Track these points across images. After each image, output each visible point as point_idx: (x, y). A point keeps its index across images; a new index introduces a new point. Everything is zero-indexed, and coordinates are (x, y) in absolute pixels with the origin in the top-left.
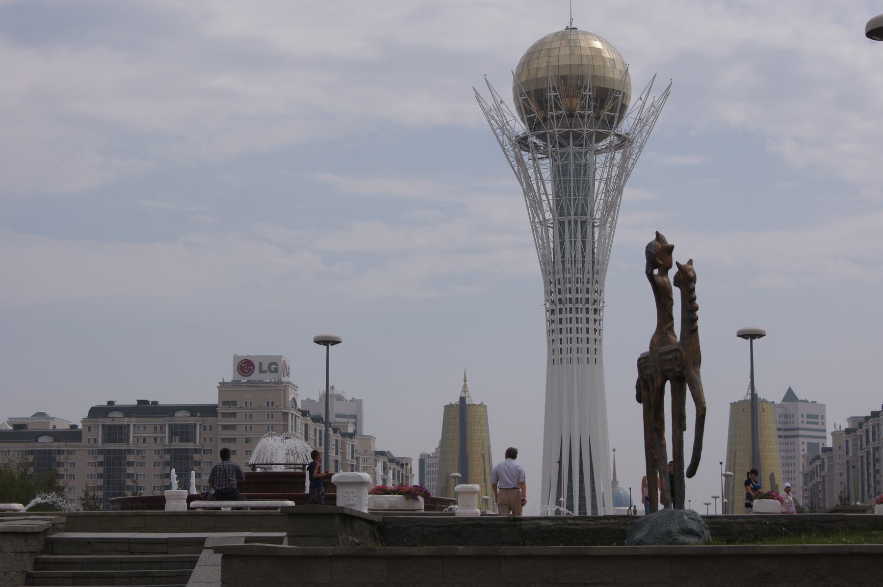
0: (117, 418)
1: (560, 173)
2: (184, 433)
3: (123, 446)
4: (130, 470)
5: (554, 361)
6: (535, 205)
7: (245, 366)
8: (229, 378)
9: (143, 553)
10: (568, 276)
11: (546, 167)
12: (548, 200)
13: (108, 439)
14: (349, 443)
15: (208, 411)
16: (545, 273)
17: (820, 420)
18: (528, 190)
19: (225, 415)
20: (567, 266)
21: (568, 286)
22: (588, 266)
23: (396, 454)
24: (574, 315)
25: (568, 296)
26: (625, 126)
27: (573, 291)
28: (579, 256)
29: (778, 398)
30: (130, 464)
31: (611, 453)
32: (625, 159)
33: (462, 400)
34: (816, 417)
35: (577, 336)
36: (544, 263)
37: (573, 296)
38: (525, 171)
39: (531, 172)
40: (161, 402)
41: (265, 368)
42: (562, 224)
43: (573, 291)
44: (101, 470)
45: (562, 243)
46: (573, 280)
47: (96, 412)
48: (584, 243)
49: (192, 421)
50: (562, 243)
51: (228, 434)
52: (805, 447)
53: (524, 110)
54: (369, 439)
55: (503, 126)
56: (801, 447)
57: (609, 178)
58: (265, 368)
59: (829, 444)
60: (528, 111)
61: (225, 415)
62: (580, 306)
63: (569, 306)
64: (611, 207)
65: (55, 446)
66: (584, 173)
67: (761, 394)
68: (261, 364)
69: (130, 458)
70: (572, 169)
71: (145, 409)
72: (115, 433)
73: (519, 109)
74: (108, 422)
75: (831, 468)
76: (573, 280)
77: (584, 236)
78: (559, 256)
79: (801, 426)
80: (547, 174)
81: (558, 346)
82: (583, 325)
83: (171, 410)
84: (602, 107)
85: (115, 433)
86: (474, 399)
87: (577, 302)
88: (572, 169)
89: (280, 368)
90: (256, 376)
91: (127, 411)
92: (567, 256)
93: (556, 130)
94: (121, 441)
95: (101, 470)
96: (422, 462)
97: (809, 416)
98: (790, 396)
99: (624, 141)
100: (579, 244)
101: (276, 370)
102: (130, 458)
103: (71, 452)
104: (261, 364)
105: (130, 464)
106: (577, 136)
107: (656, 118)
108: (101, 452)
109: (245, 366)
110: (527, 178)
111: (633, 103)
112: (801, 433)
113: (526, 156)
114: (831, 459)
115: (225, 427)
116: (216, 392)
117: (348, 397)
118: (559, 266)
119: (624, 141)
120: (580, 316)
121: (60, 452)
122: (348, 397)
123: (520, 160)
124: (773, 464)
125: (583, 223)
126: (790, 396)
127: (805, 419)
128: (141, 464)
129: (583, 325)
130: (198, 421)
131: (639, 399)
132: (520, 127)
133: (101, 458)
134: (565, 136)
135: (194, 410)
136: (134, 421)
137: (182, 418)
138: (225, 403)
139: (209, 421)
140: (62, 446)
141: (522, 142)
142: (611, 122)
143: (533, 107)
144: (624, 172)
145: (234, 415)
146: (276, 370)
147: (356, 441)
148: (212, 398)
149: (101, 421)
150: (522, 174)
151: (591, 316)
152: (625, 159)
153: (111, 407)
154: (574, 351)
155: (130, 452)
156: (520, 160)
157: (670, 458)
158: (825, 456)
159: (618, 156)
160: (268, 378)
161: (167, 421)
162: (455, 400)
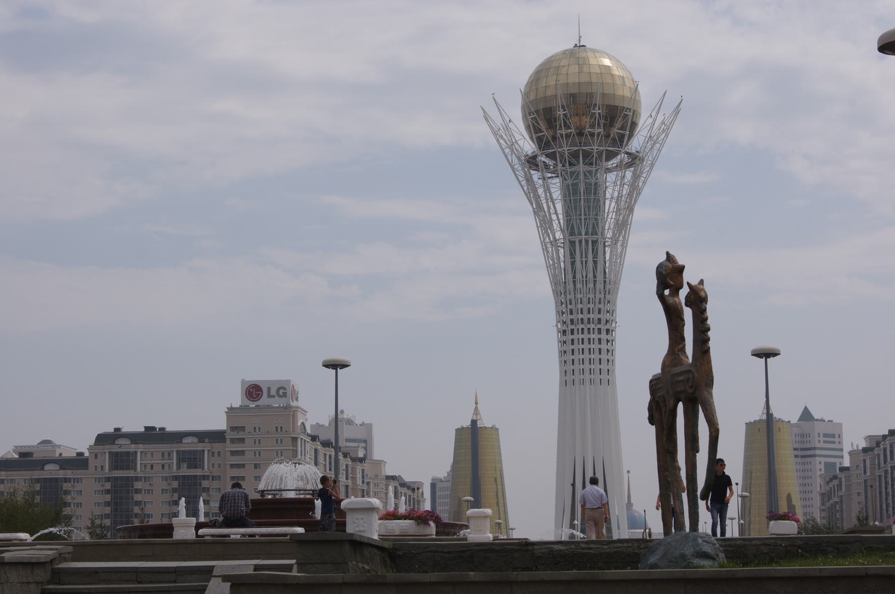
0: (124, 445)
1: (570, 193)
2: (192, 459)
3: (130, 473)
4: (138, 497)
5: (564, 383)
6: (545, 224)
7: (253, 391)
8: (237, 403)
11: (556, 186)
13: (115, 466)
14: (359, 467)
15: (216, 436)
16: (556, 293)
17: (837, 440)
18: (538, 210)
19: (233, 441)
20: (579, 286)
21: (580, 306)
22: (599, 286)
24: (586, 336)
25: (580, 316)
26: (636, 144)
27: (585, 311)
28: (591, 275)
29: (793, 417)
30: (138, 491)
31: (626, 475)
32: (636, 177)
33: (474, 422)
34: (833, 436)
35: (589, 356)
36: (555, 283)
37: (585, 316)
38: (535, 190)
39: (541, 191)
40: (170, 428)
41: (273, 392)
42: (572, 243)
43: (585, 311)
44: (108, 497)
46: (585, 300)
47: (102, 439)
48: (595, 263)
49: (200, 447)
51: (236, 460)
53: (533, 129)
54: (380, 463)
55: (512, 145)
56: (818, 466)
57: (620, 196)
58: (273, 392)
59: (847, 463)
60: (537, 130)
61: (233, 441)
62: (592, 326)
63: (581, 326)
64: (622, 226)
65: (61, 474)
66: (594, 192)
67: (777, 413)
68: (269, 389)
69: (138, 485)
71: (152, 435)
72: (122, 461)
73: (528, 128)
74: (115, 449)
75: (848, 487)
76: (585, 300)
77: (595, 256)
78: (570, 277)
79: (818, 445)
80: (557, 194)
83: (178, 437)
85: (122, 461)
86: (486, 421)
87: (589, 322)
89: (289, 392)
90: (264, 401)
91: (134, 438)
92: (578, 276)
94: (128, 468)
95: (108, 497)
96: (433, 486)
97: (825, 435)
98: (806, 415)
99: (634, 159)
100: (590, 264)
102: (138, 485)
103: (78, 480)
104: (269, 389)
105: (138, 491)
106: (587, 155)
108: (108, 479)
109: (253, 391)
110: (537, 197)
111: (644, 122)
113: (535, 175)
114: (848, 478)
115: (233, 453)
116: (224, 417)
117: (358, 421)
118: (570, 286)
119: (634, 159)
120: (592, 336)
121: (66, 480)
122: (358, 421)
123: (529, 180)
124: (789, 482)
125: (594, 243)
126: (806, 415)
127: (822, 439)
130: (206, 447)
131: (652, 420)
132: (529, 147)
134: (575, 155)
135: (202, 436)
136: (140, 448)
137: (189, 444)
138: (233, 429)
139: (217, 447)
140: (69, 474)
141: (532, 162)
142: (621, 141)
144: (635, 190)
146: (285, 395)
147: (366, 466)
148: (219, 423)
149: (108, 448)
151: (604, 336)
152: (636, 177)
153: (118, 434)
154: (587, 372)
155: (137, 479)
156: (529, 180)
158: (842, 476)
159: (629, 174)
160: (276, 403)
161: (175, 448)
162: (467, 423)
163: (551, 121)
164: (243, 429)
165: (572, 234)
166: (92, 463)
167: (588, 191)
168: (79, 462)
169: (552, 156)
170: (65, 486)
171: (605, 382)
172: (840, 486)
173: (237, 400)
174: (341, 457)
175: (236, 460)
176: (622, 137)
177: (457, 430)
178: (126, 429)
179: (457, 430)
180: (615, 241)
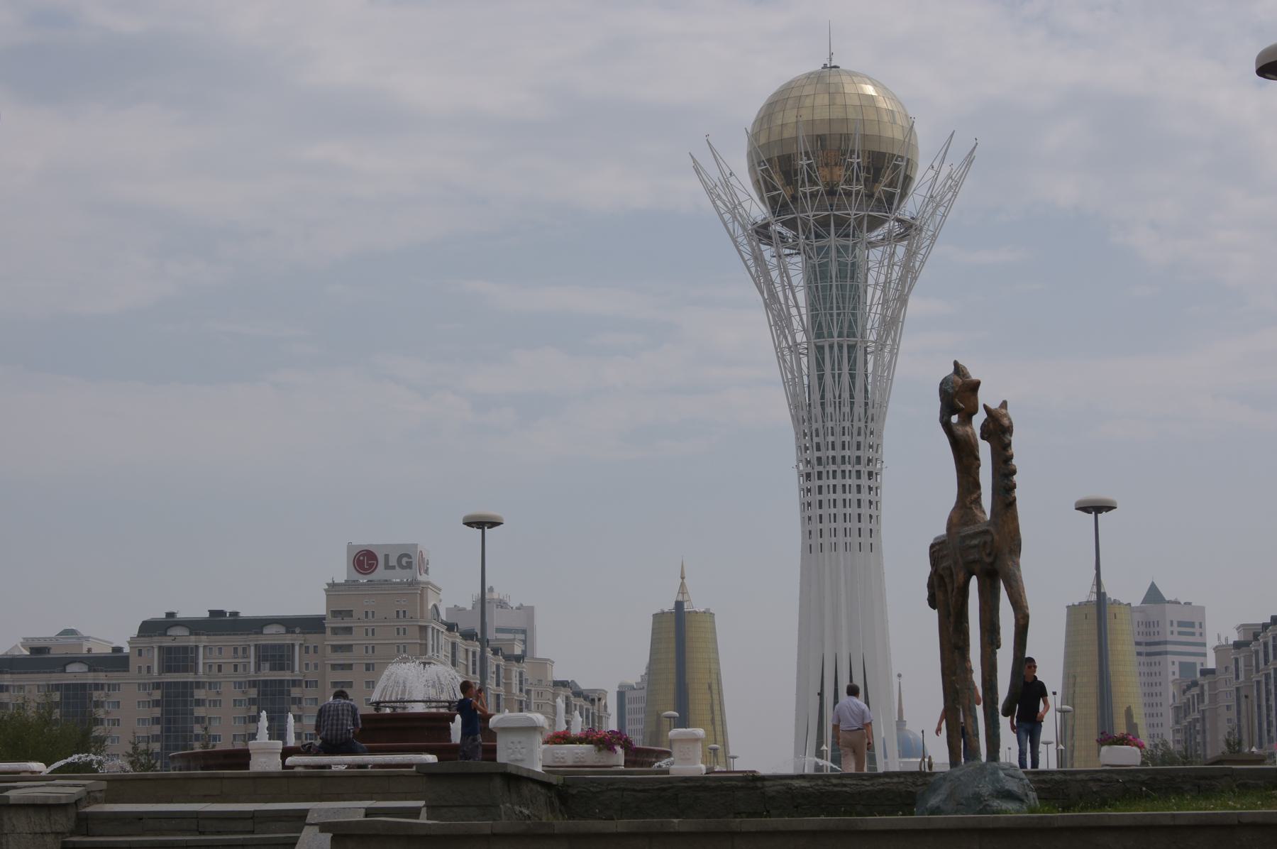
0: (180, 637)
1: (817, 276)
2: (277, 657)
3: (189, 677)
4: (199, 711)
6: (781, 322)
7: (365, 560)
8: (341, 578)
9: (219, 833)
10: (830, 424)
13: (167, 667)
14: (515, 669)
15: (312, 625)
16: (797, 421)
17: (1197, 630)
18: (771, 301)
19: (335, 631)
20: (829, 410)
22: (859, 410)
23: (584, 685)
24: (839, 482)
25: (831, 453)
26: (910, 207)
28: (846, 395)
30: (199, 703)
32: (911, 254)
33: (679, 605)
34: (1192, 625)
37: (838, 453)
38: (766, 273)
39: (775, 274)
40: (245, 613)
41: (393, 562)
42: (820, 349)
44: (157, 712)
45: (821, 377)
46: (838, 430)
47: (149, 628)
48: (852, 377)
49: (288, 639)
50: (821, 377)
51: (341, 658)
52: (1176, 668)
53: (765, 186)
54: (544, 664)
55: (734, 208)
56: (1171, 668)
58: (393, 562)
59: (1211, 663)
60: (770, 187)
61: (335, 631)
62: (848, 467)
63: (832, 468)
64: (891, 324)
66: (851, 274)
67: (1111, 592)
68: (387, 556)
69: (200, 694)
70: (834, 269)
74: (167, 642)
75: (1214, 698)
76: (838, 430)
77: (852, 367)
78: (816, 396)
79: (1170, 638)
80: (798, 278)
81: (816, 526)
82: (852, 496)
83: (257, 625)
84: (876, 179)
85: (177, 659)
86: (696, 604)
88: (834, 269)
89: (415, 561)
90: (380, 574)
91: (195, 626)
92: (829, 395)
93: (811, 214)
95: (157, 712)
96: (621, 695)
97: (1181, 624)
98: (1153, 595)
99: (908, 229)
100: (846, 379)
101: (409, 565)
102: (200, 694)
104: (387, 556)
105: (199, 703)
106: (841, 222)
107: (955, 195)
108: (157, 686)
109: (365, 560)
110: (770, 283)
111: (922, 175)
112: (1170, 648)
113: (767, 252)
114: (1213, 686)
115: (336, 648)
117: (514, 603)
118: (817, 410)
119: (908, 229)
120: (848, 482)
121: (98, 687)
122: (514, 603)
123: (758, 258)
125: (852, 348)
126: (1153, 595)
127: (1176, 629)
128: (215, 703)
129: (852, 496)
130: (297, 639)
132: (757, 210)
133: (157, 695)
134: (824, 223)
136: (203, 641)
137: (273, 635)
138: (336, 613)
139: (313, 639)
140: (101, 677)
141: (762, 232)
142: (889, 202)
143: (778, 181)
145: (348, 630)
146: (409, 565)
147: (525, 667)
148: (317, 607)
149: (158, 641)
151: (864, 481)
152: (911, 254)
153: (171, 621)
155: (199, 685)
156: (758, 258)
158: (1205, 682)
159: (900, 250)
160: (398, 576)
161: (252, 640)
162: (669, 606)
163: (789, 175)
164: (349, 613)
165: (819, 335)
166: (134, 663)
167: (842, 274)
168: (116, 661)
169: (791, 224)
170: (97, 695)
171: (866, 547)
172: (1201, 696)
173: (341, 571)
175: (341, 658)
177: (655, 616)
178: (181, 615)
179: (655, 616)
180: (880, 345)
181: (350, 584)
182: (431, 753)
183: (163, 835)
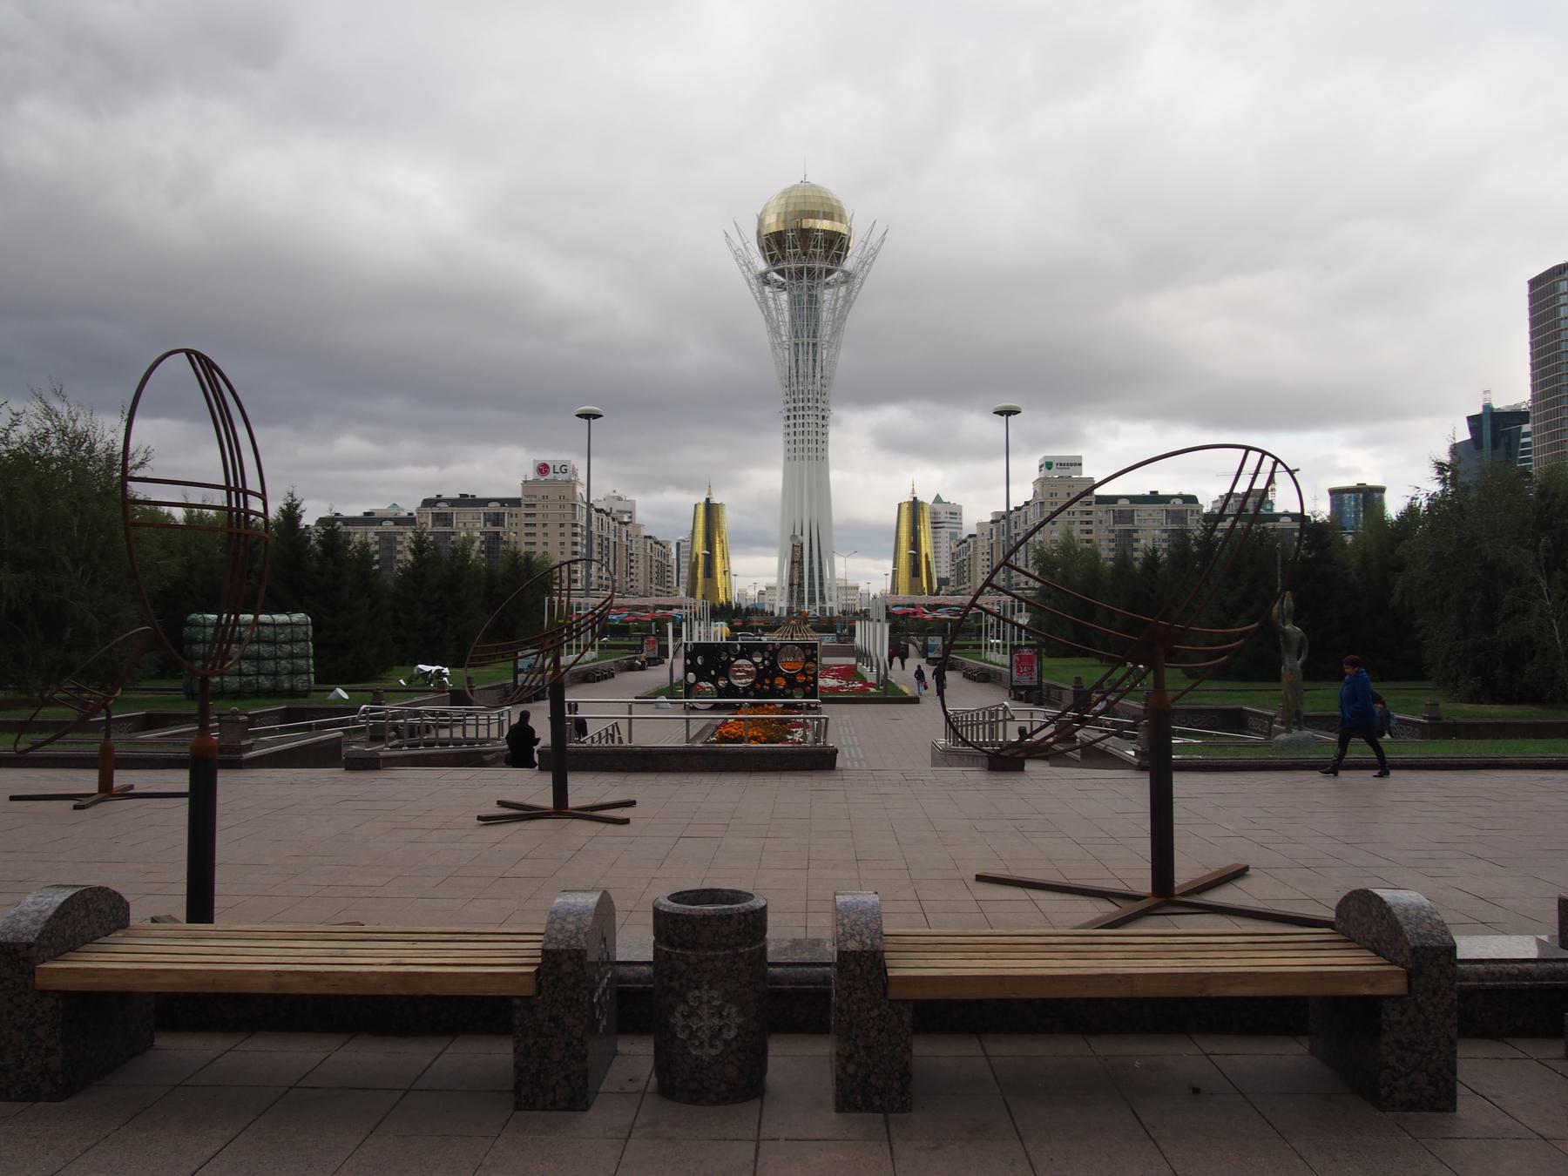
0: (443, 508)
1: (794, 302)
6: (775, 331)
7: (543, 469)
11: (784, 296)
12: (785, 330)
14: (624, 528)
15: (515, 502)
19: (527, 505)
26: (849, 264)
32: (849, 292)
37: (806, 437)
39: (771, 303)
40: (479, 496)
47: (427, 503)
49: (501, 510)
51: (530, 520)
54: (639, 526)
55: (748, 264)
57: (834, 309)
60: (770, 249)
61: (527, 505)
64: (836, 331)
66: (813, 300)
71: (466, 501)
73: (762, 248)
74: (435, 510)
77: (815, 353)
78: (794, 372)
80: (785, 306)
83: (485, 502)
84: (830, 247)
86: (715, 500)
88: (805, 298)
90: (551, 476)
91: (453, 503)
98: (938, 499)
99: (848, 277)
105: (804, 563)
106: (810, 271)
109: (543, 469)
110: (768, 307)
113: (767, 289)
118: (794, 380)
119: (848, 277)
123: (762, 293)
126: (938, 499)
130: (506, 510)
132: (761, 265)
134: (800, 272)
135: (502, 502)
136: (456, 510)
137: (494, 508)
139: (515, 510)
141: (764, 279)
142: (839, 258)
144: (848, 302)
145: (534, 505)
147: (630, 527)
148: (517, 493)
150: (763, 302)
151: (820, 421)
152: (849, 292)
156: (762, 293)
157: (244, 743)
158: (970, 540)
159: (843, 289)
160: (561, 477)
161: (481, 510)
167: (810, 302)
169: (781, 272)
173: (531, 474)
174: (594, 515)
175: (530, 520)
176: (839, 257)
178: (445, 496)
181: (535, 481)
182: (1520, 931)
183: (174, 725)
